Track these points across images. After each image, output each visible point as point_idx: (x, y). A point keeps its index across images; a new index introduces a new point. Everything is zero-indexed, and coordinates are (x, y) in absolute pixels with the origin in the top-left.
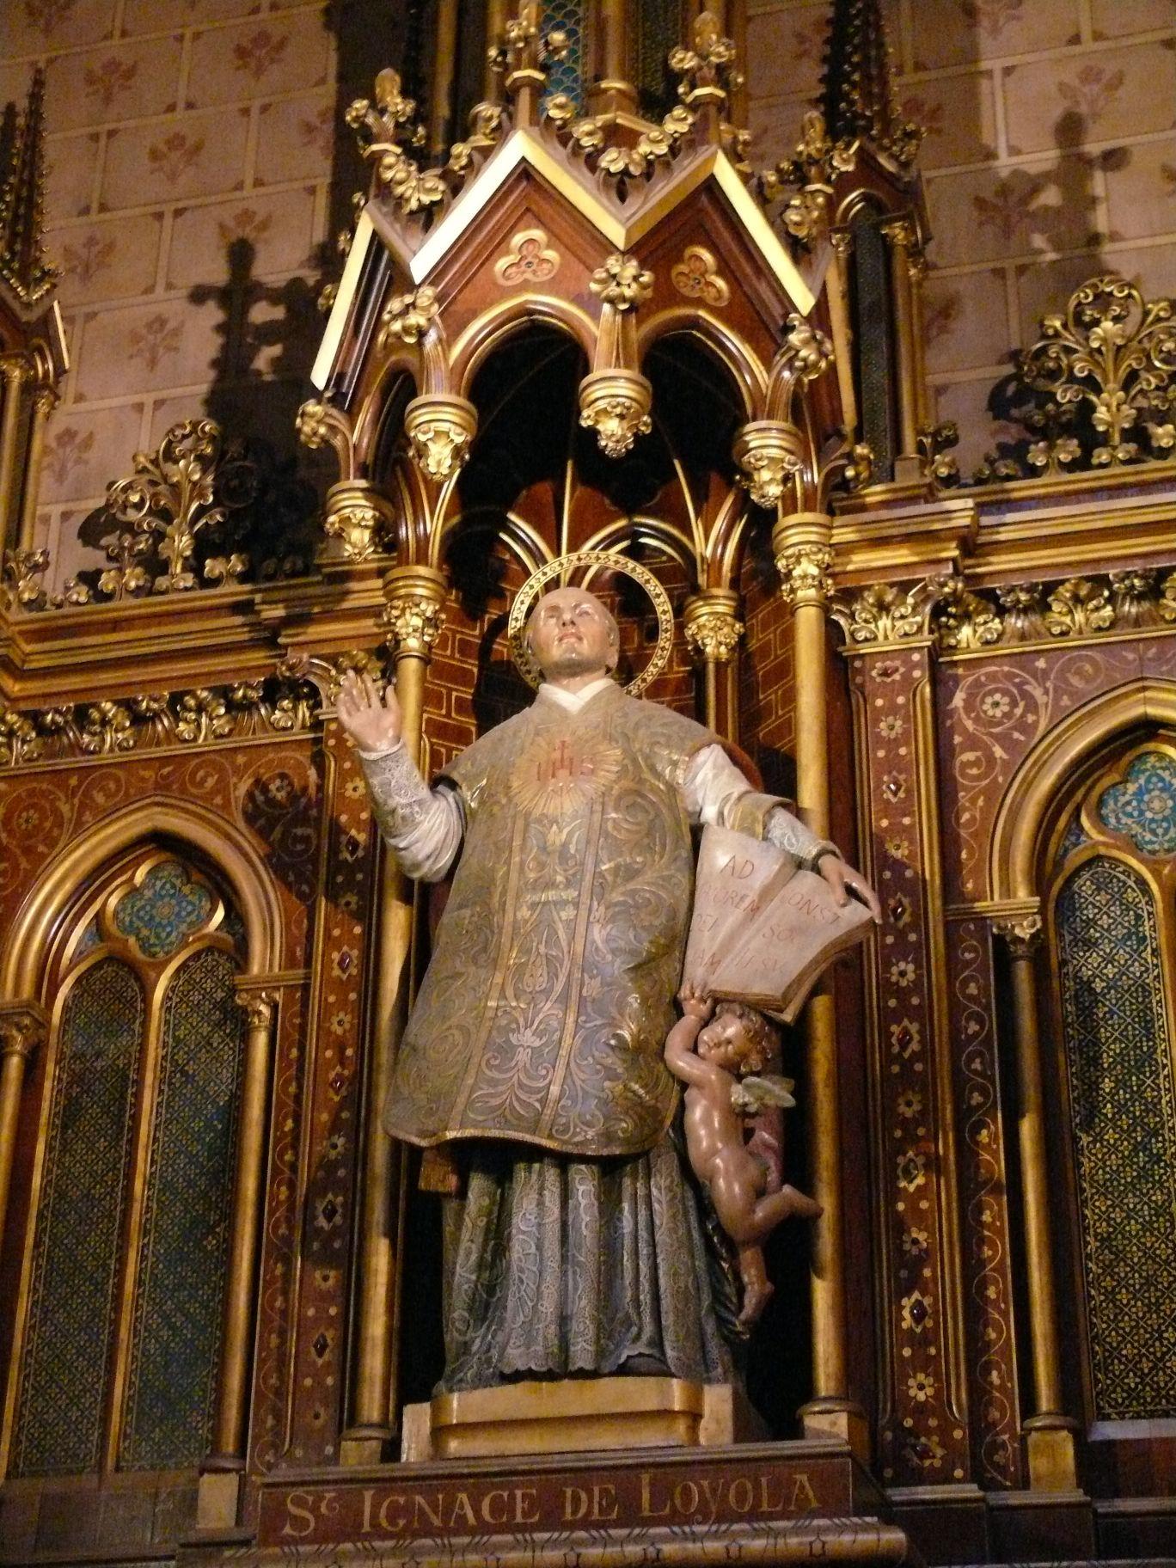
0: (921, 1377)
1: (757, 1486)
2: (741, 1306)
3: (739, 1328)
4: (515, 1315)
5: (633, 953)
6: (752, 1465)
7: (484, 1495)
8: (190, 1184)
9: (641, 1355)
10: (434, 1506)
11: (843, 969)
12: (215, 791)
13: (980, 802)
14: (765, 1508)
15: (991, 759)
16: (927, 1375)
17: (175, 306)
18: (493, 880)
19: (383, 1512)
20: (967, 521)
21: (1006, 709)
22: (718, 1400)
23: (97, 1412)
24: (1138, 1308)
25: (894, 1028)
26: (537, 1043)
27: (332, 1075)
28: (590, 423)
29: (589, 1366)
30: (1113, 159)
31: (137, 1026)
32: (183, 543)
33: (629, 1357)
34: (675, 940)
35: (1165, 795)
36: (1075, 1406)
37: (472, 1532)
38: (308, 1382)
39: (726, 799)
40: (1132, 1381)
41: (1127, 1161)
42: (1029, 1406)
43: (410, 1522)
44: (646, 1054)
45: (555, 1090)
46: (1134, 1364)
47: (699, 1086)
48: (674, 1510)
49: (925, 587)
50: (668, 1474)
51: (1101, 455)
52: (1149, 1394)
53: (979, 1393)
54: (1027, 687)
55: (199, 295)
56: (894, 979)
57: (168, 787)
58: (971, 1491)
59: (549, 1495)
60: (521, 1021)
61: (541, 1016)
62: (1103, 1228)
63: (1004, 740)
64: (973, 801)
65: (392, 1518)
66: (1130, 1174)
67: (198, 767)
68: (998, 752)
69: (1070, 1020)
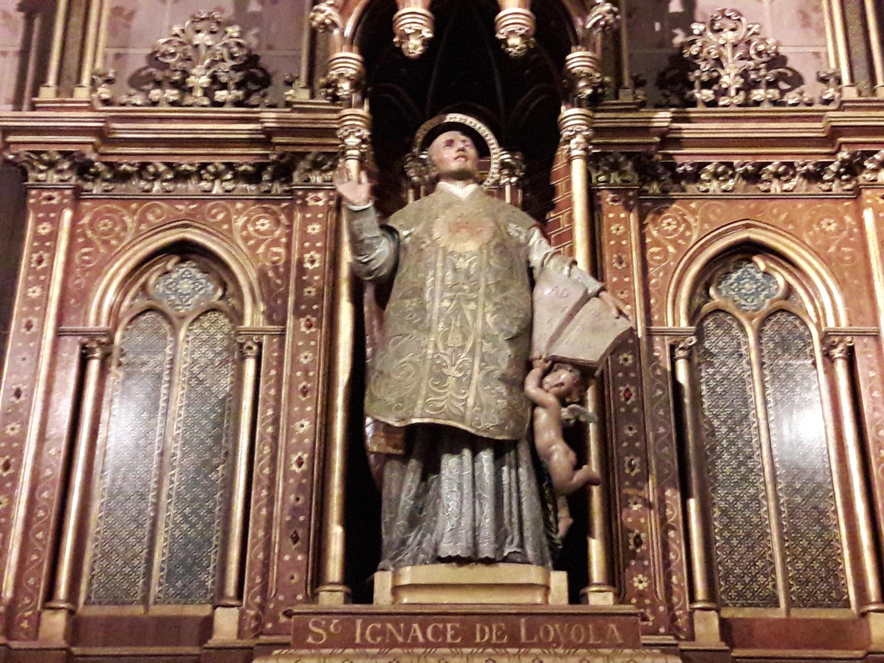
0: (640, 576)
1: (587, 629)
2: (557, 531)
3: (558, 541)
5: (509, 333)
6: (583, 618)
7: (429, 625)
8: (202, 442)
9: (515, 552)
10: (399, 631)
12: (223, 222)
13: (661, 274)
14: (591, 641)
15: (666, 251)
16: (644, 576)
18: (424, 284)
19: (368, 632)
20: (666, 124)
21: (674, 227)
23: (142, 570)
24: (742, 549)
25: (622, 388)
26: (459, 375)
27: (301, 386)
28: (502, 37)
29: (492, 556)
31: (168, 351)
32: (200, 79)
33: (510, 553)
35: (752, 282)
37: (422, 646)
38: (287, 558)
39: (546, 255)
40: (740, 587)
41: (736, 470)
42: (693, 599)
43: (383, 640)
45: (471, 402)
46: (740, 577)
47: (544, 406)
48: (540, 639)
49: (640, 157)
50: (536, 617)
51: (723, 101)
52: (749, 595)
54: (686, 217)
56: (621, 362)
57: (193, 216)
59: (467, 626)
60: (448, 362)
61: (460, 361)
62: (723, 504)
63: (674, 243)
64: (658, 273)
65: (374, 634)
66: (736, 478)
67: (213, 208)
68: (671, 249)
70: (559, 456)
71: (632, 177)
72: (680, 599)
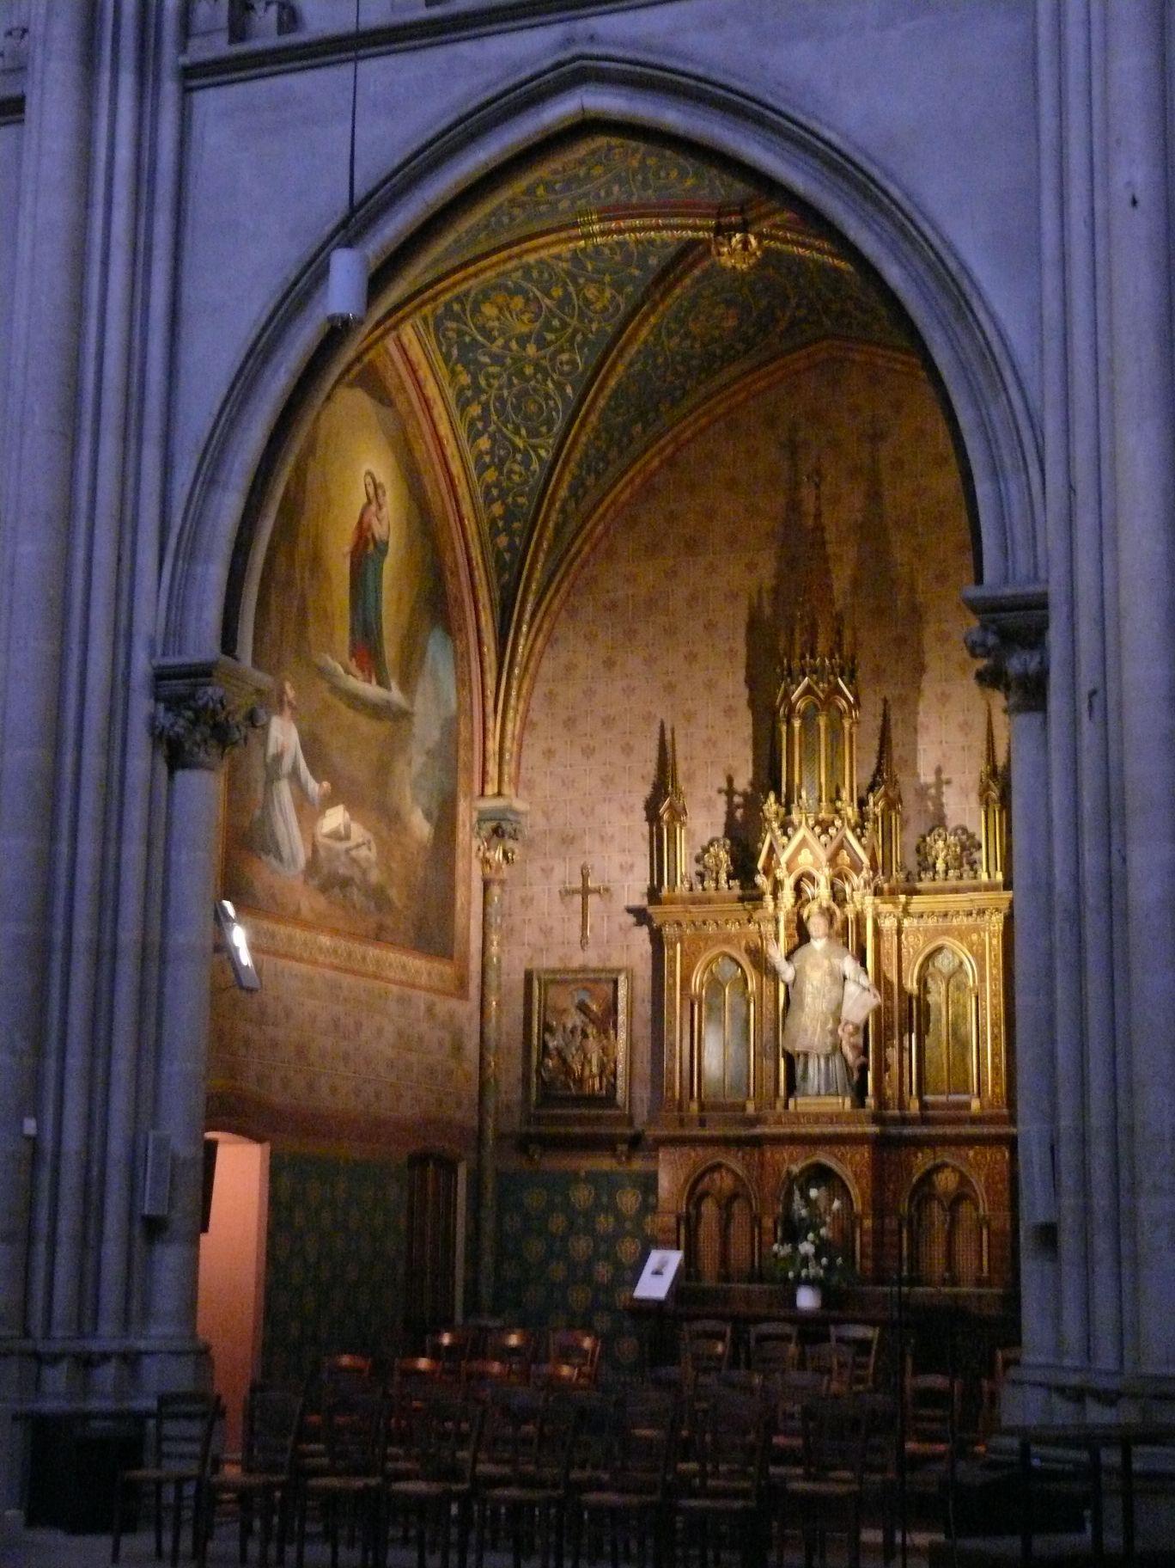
4: (810, 1083)
11: (877, 1012)
17: (714, 794)
22: (848, 1102)
30: (948, 782)
34: (840, 1006)
36: (920, 1094)
44: (834, 1032)
50: (838, 1115)
53: (901, 1090)
55: (720, 791)
69: (925, 1010)
70: (850, 1056)
72: (906, 1096)
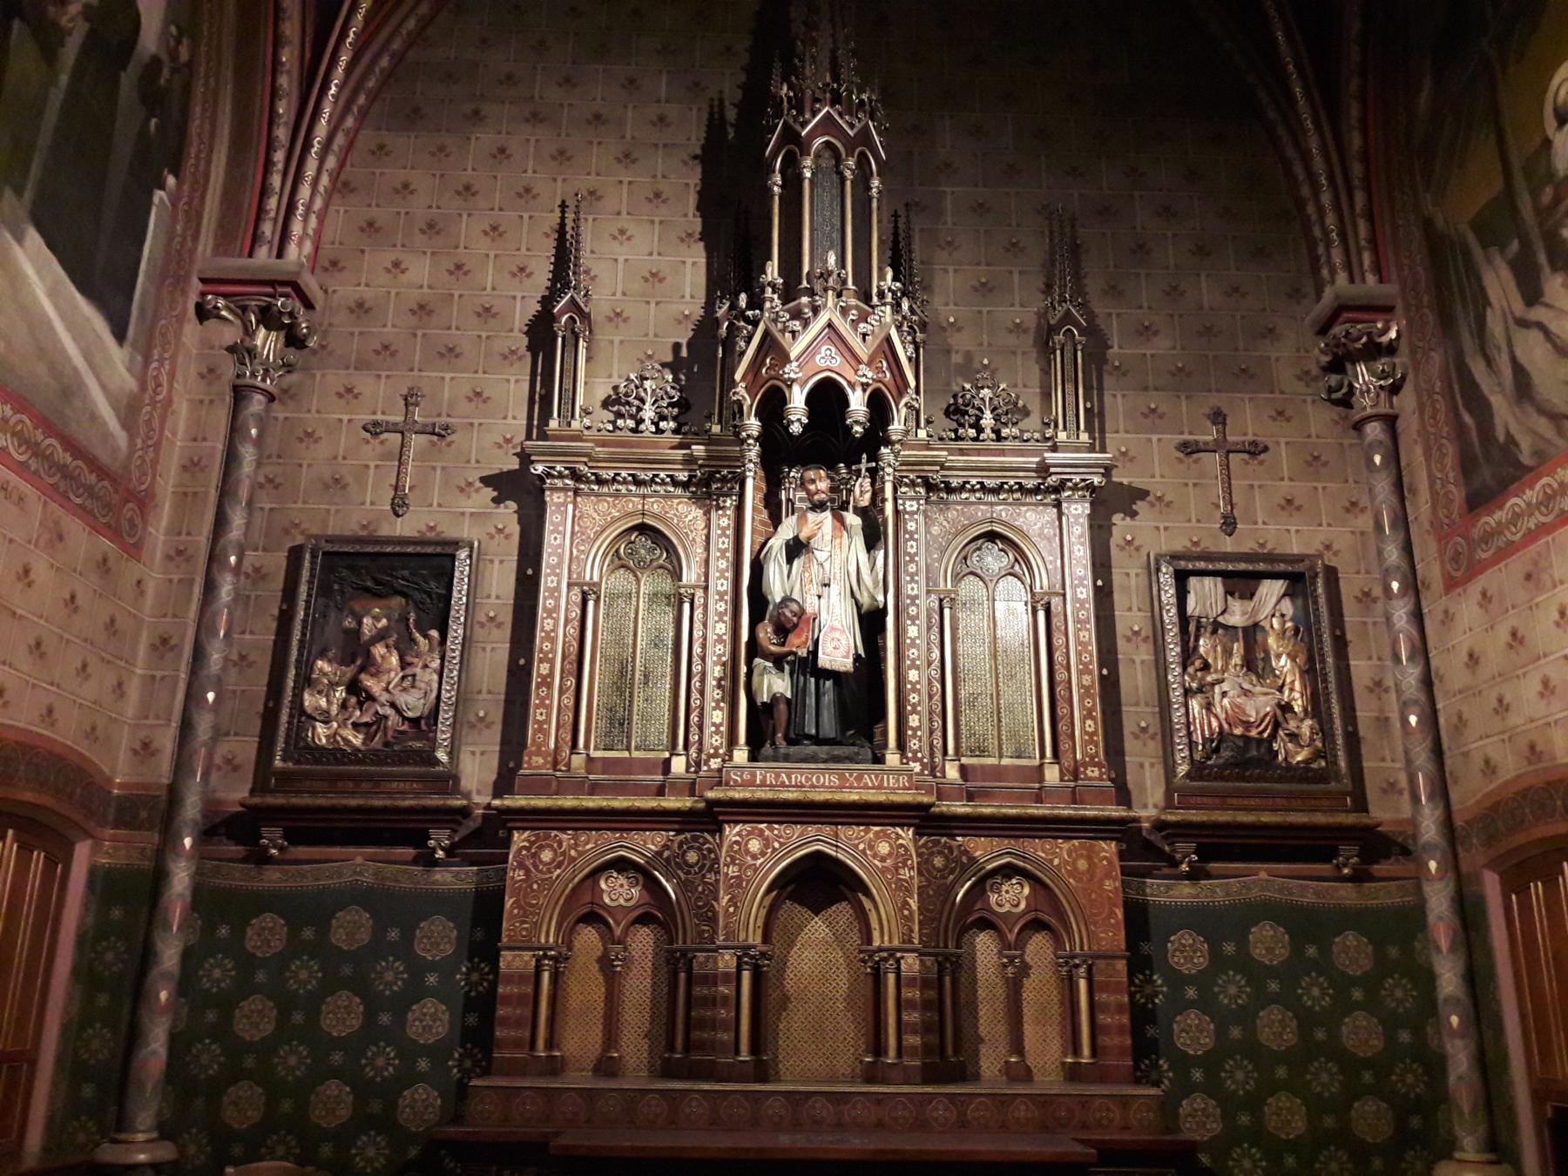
32: (648, 413)
58: (930, 778)
71: (922, 490)
